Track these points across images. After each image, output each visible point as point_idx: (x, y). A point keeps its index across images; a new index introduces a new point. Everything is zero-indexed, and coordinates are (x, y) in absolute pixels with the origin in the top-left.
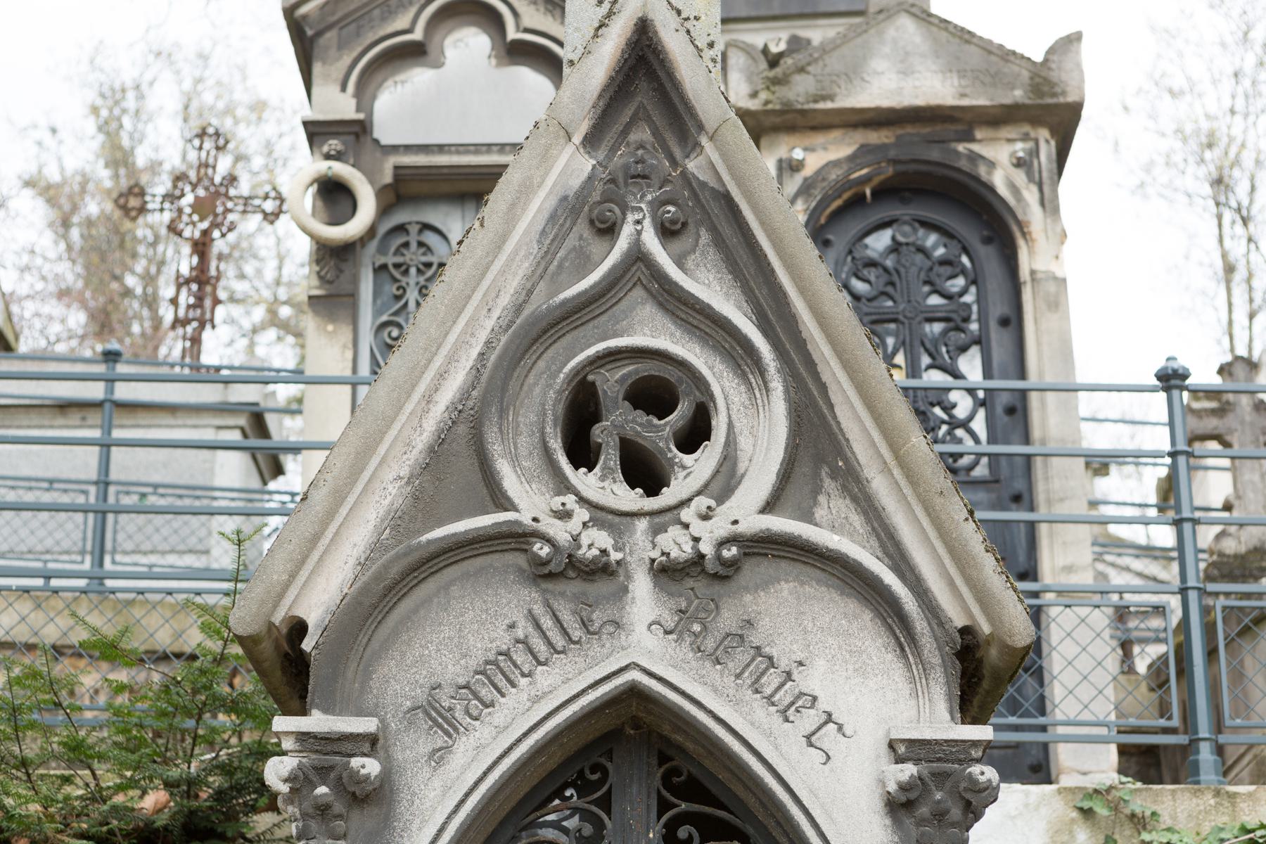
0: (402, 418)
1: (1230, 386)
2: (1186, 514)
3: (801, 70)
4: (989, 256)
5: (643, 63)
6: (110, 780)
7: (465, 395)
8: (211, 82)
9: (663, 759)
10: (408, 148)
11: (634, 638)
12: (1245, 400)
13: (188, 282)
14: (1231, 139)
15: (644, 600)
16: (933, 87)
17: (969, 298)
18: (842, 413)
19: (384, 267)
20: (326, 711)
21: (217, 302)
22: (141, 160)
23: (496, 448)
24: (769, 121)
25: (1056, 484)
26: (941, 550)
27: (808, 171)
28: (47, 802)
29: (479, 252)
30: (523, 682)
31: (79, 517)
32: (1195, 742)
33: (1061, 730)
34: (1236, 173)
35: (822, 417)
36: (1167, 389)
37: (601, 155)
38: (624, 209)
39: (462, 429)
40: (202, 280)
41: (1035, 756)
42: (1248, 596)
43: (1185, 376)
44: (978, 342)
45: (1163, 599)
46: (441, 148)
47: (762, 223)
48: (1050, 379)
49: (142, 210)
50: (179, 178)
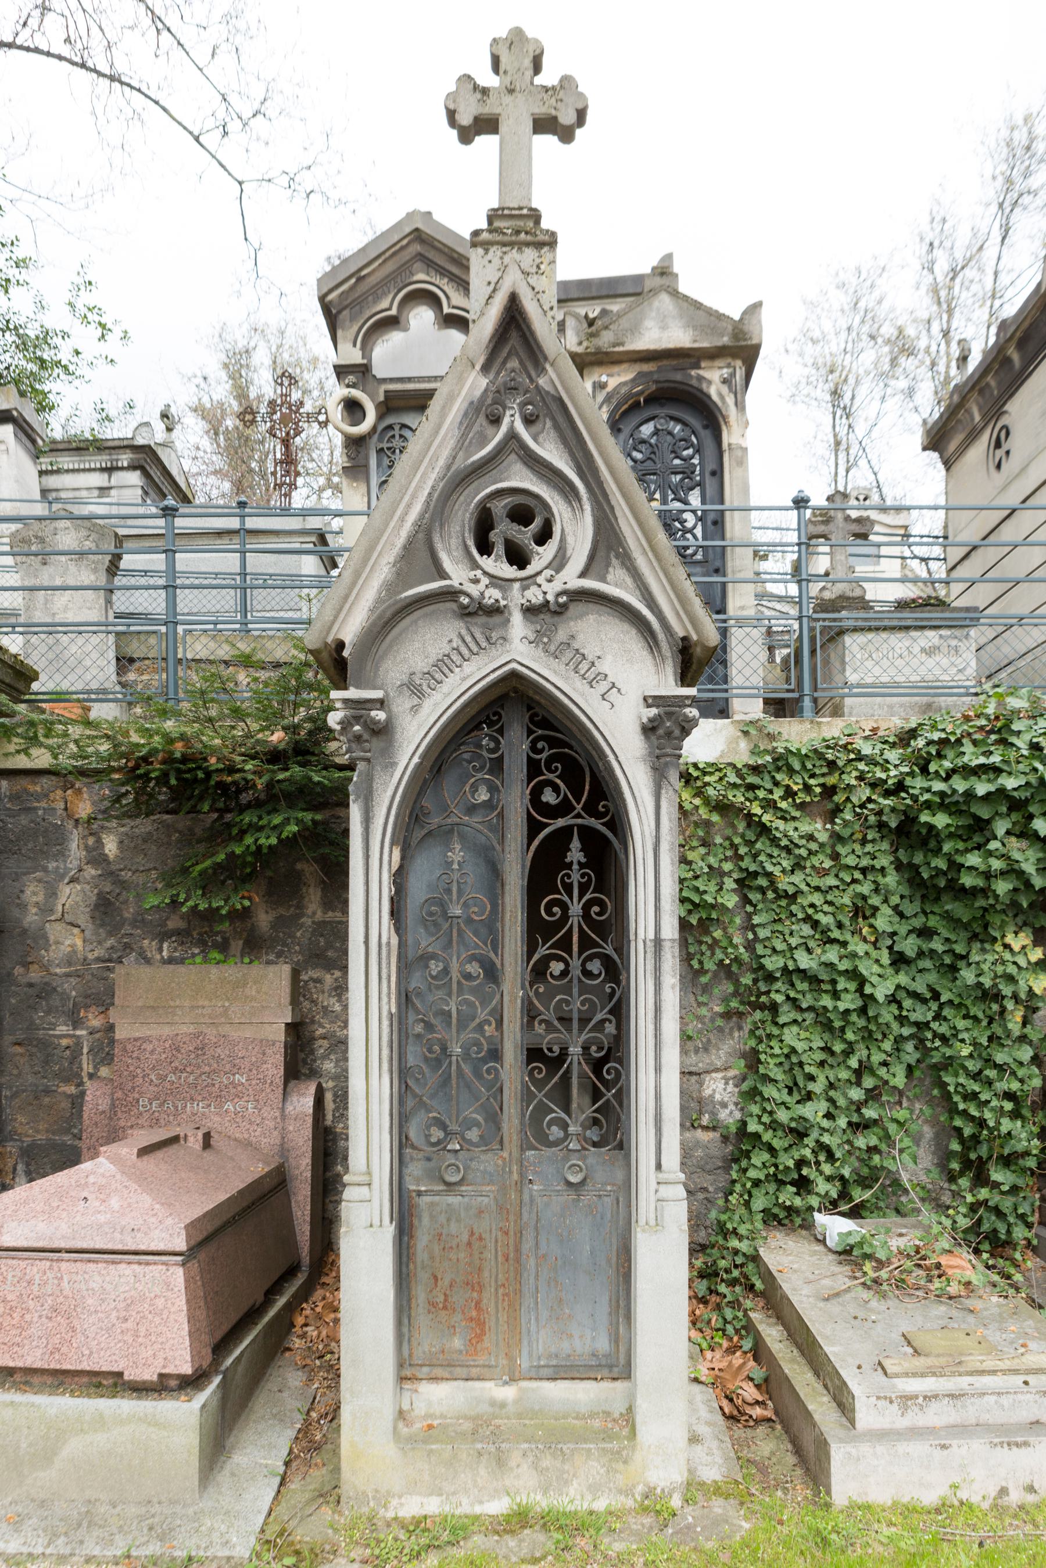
0: (389, 530)
1: (832, 506)
2: (804, 577)
3: (606, 328)
4: (706, 435)
5: (514, 320)
6: (255, 726)
7: (422, 516)
8: (287, 347)
9: (529, 708)
10: (392, 380)
11: (513, 646)
12: (840, 515)
13: (281, 462)
14: (843, 367)
15: (518, 626)
16: (677, 336)
17: (696, 461)
18: (621, 522)
19: (382, 449)
20: (357, 687)
21: (298, 474)
22: (252, 395)
23: (439, 546)
24: (588, 359)
25: (738, 563)
26: (673, 596)
27: (609, 389)
28: (223, 738)
29: (426, 435)
30: (457, 670)
31: (232, 592)
32: (802, 696)
33: (735, 691)
34: (845, 388)
35: (609, 521)
36: (798, 508)
37: (492, 376)
38: (505, 408)
39: (421, 536)
40: (289, 461)
41: (722, 704)
42: (835, 620)
43: (807, 501)
44: (699, 484)
45: (791, 622)
46: (409, 380)
47: (580, 415)
48: (736, 504)
49: (253, 421)
50: (272, 403)
